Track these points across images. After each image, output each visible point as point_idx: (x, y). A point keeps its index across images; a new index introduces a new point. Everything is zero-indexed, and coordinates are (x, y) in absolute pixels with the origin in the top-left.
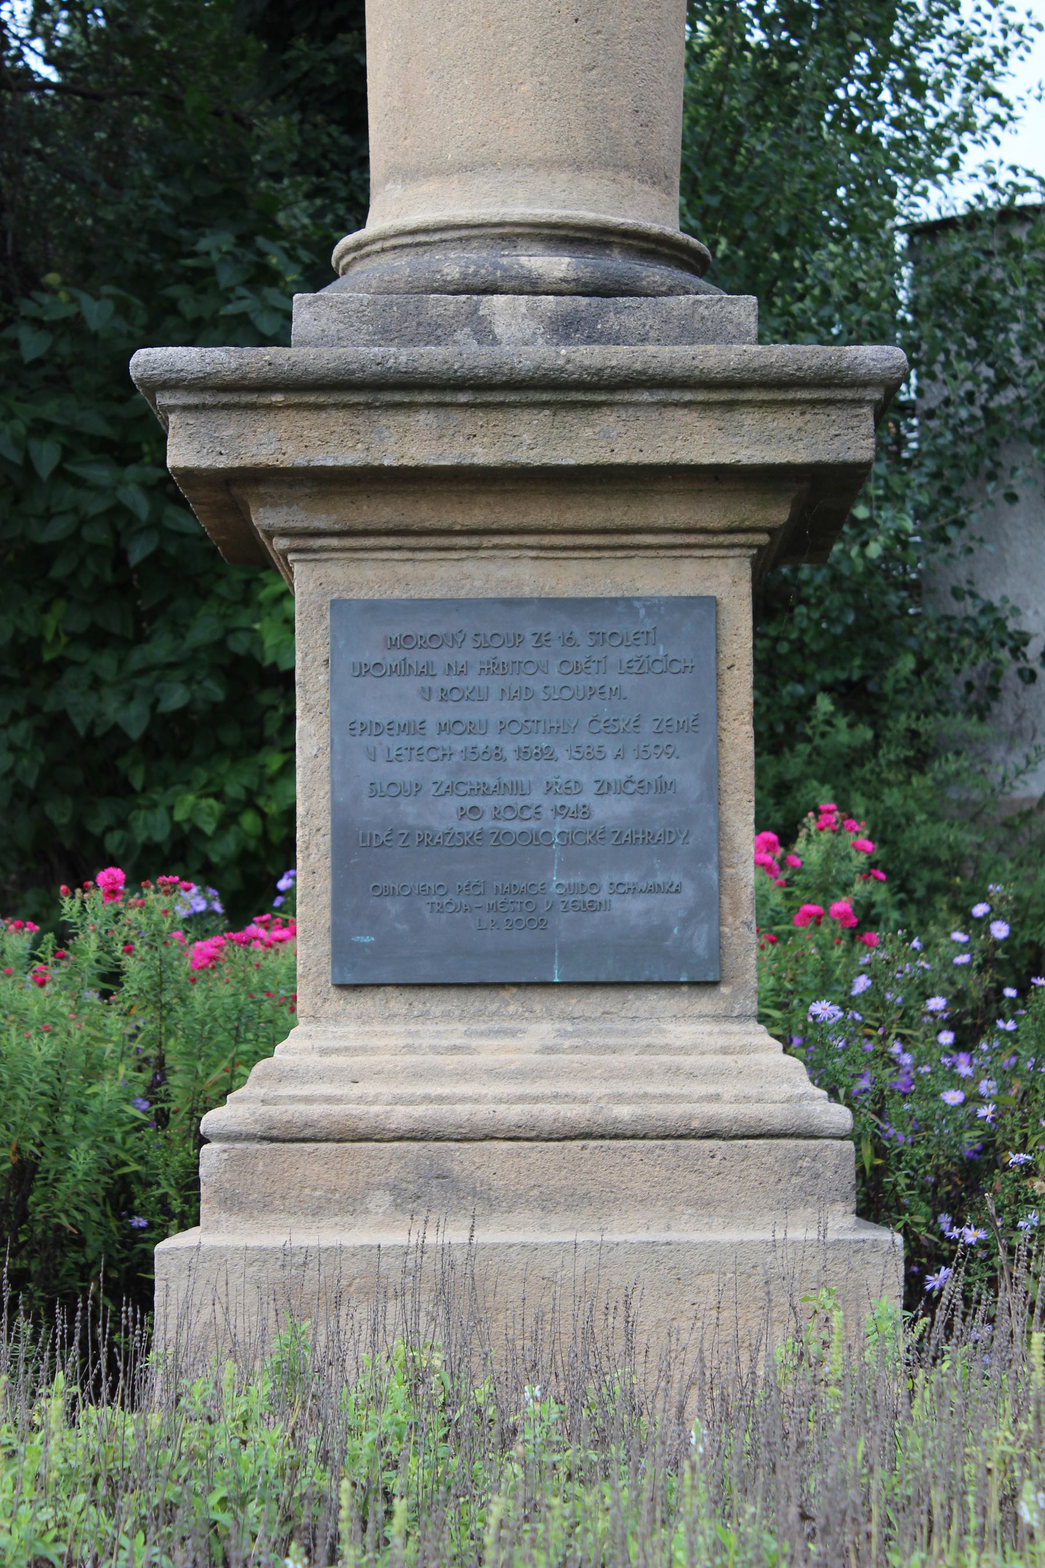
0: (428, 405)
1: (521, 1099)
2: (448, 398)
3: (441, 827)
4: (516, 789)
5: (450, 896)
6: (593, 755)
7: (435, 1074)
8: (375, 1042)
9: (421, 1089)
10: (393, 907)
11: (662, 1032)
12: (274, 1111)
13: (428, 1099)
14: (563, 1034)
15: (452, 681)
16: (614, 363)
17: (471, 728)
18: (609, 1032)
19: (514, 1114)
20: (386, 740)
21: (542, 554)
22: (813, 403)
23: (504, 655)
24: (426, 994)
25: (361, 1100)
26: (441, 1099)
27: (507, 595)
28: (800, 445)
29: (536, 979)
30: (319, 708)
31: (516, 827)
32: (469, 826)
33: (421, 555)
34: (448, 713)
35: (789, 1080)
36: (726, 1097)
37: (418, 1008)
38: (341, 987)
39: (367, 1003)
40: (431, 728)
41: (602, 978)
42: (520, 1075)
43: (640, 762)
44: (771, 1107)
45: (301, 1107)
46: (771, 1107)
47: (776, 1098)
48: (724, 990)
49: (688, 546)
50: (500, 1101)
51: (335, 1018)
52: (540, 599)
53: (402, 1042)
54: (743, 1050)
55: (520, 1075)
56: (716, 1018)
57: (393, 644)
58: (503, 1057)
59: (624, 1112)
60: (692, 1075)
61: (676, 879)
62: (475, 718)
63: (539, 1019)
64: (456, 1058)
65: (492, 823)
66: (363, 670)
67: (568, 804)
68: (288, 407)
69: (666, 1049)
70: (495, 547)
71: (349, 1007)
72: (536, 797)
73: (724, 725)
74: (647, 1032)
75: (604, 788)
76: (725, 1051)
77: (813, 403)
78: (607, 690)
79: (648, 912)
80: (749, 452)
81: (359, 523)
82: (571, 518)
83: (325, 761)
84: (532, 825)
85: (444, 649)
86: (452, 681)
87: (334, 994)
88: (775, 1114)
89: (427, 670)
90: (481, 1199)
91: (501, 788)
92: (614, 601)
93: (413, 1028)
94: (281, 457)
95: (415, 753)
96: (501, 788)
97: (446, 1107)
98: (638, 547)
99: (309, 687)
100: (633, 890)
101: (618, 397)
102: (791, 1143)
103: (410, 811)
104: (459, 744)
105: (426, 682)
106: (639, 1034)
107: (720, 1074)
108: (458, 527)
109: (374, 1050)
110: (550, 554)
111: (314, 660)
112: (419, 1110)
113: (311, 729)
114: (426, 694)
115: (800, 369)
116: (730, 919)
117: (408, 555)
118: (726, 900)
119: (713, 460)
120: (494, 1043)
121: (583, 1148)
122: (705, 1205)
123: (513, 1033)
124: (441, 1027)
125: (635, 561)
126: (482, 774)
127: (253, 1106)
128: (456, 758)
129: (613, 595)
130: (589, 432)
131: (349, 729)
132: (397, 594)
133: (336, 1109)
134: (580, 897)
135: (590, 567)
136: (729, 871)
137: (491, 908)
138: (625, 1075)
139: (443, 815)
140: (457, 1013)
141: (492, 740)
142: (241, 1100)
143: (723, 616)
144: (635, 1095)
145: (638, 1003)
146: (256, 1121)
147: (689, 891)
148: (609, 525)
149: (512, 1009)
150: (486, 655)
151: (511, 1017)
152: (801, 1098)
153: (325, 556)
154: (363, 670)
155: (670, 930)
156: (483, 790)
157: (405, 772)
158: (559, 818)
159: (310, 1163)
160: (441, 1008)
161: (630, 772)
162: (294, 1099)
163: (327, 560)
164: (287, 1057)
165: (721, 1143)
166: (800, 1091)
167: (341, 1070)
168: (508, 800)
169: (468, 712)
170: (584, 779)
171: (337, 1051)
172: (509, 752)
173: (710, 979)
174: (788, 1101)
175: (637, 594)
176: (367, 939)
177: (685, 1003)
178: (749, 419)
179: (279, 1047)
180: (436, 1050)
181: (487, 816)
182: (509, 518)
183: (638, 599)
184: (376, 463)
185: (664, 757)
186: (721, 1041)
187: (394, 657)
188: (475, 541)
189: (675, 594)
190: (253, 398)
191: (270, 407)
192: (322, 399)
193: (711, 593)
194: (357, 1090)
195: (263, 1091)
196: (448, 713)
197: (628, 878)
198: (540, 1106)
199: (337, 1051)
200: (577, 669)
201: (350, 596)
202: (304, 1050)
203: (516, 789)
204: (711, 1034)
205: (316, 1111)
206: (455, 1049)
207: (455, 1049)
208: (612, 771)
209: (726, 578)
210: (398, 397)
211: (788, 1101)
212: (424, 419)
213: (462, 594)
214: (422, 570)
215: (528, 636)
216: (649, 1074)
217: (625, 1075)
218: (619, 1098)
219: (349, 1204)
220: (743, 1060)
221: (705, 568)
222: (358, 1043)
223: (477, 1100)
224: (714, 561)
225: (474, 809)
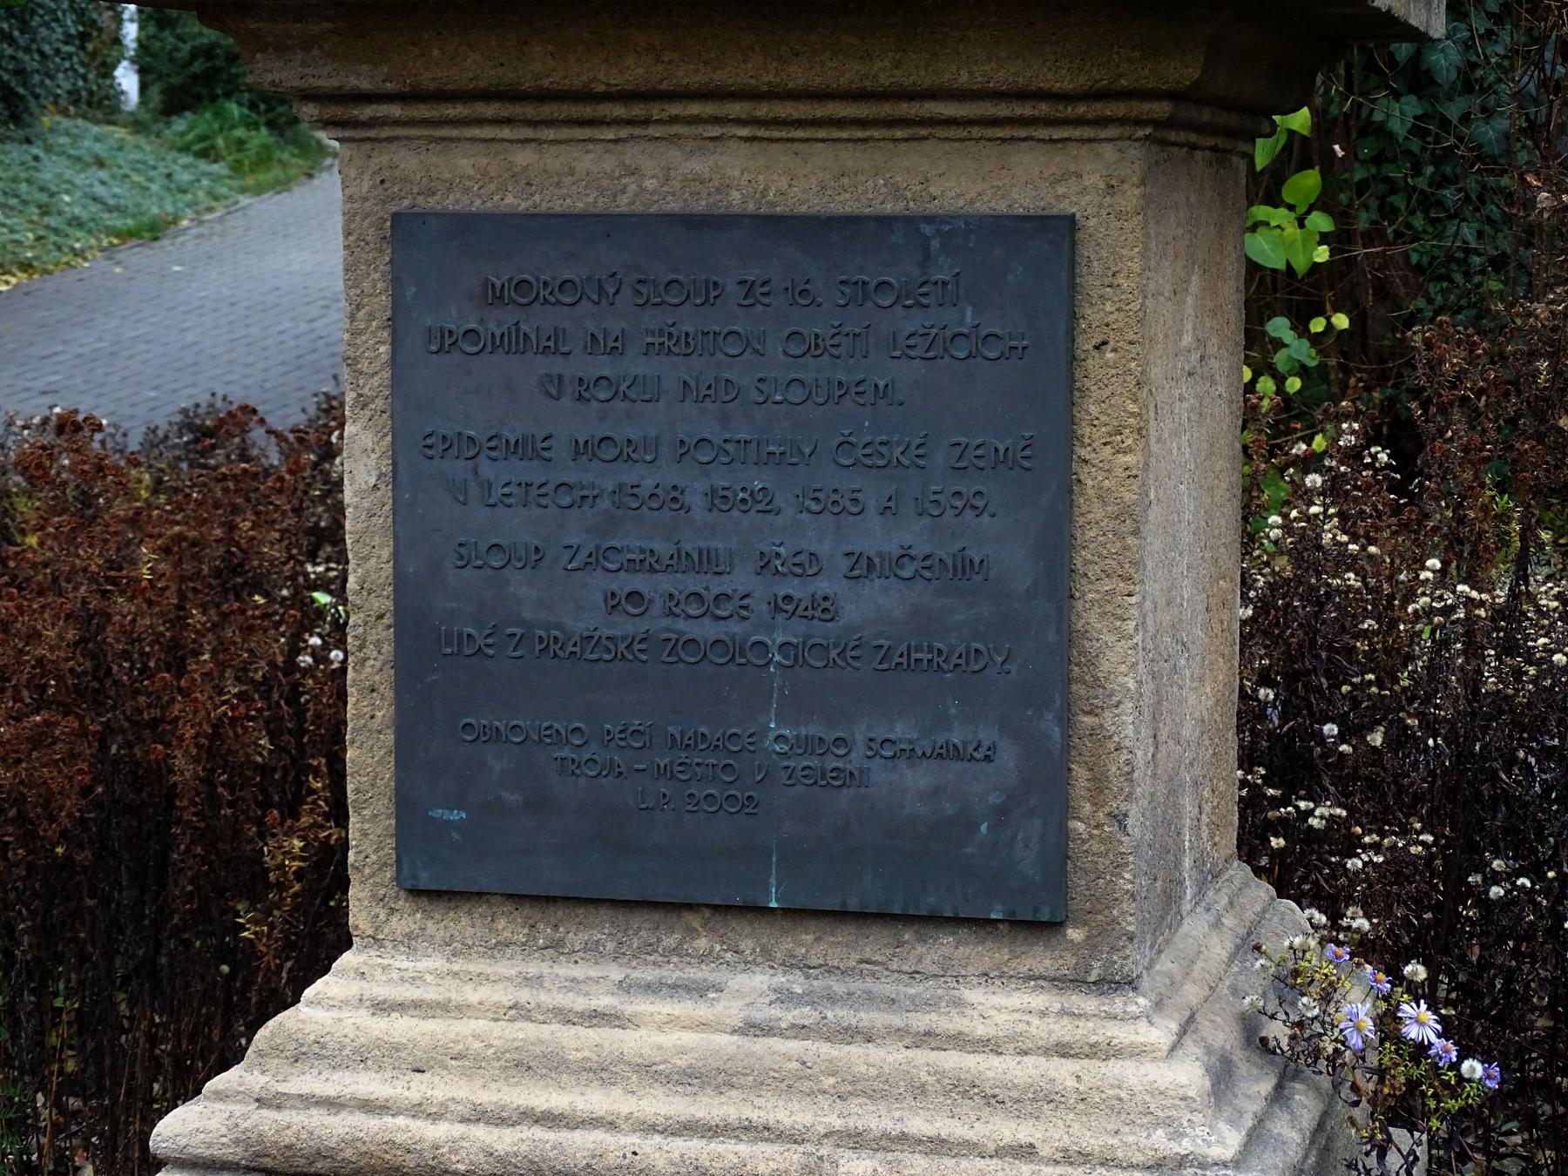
1: (688, 1128)
3: (580, 625)
4: (707, 562)
5: (593, 747)
6: (841, 508)
7: (552, 1066)
10: (497, 762)
11: (959, 1003)
12: (268, 1122)
14: (784, 997)
17: (628, 453)
18: (870, 999)
21: (761, 133)
23: (688, 321)
25: (417, 1110)
26: (550, 1119)
27: (700, 206)
29: (738, 901)
30: (380, 402)
31: (707, 630)
32: (624, 627)
33: (551, 134)
35: (1168, 1122)
36: (1045, 1151)
37: (545, 933)
38: (415, 893)
39: (463, 924)
40: (561, 451)
41: (853, 905)
42: (693, 1078)
43: (926, 520)
48: (1074, 934)
49: (1022, 122)
50: (649, 1128)
51: (409, 942)
52: (756, 217)
53: (507, 1000)
55: (693, 1078)
56: (1060, 983)
57: (494, 297)
60: (993, 1101)
61: (987, 735)
62: (634, 433)
63: (749, 965)
65: (665, 622)
66: (445, 341)
67: (797, 595)
69: (959, 1041)
70: (674, 120)
72: (741, 580)
74: (930, 1004)
75: (863, 567)
76: (1063, 1051)
78: (867, 387)
79: (937, 791)
81: (427, 79)
82: (798, 75)
84: (736, 628)
85: (586, 306)
89: (553, 345)
91: (682, 561)
92: (886, 221)
93: (533, 969)
95: (534, 491)
96: (682, 561)
99: (363, 365)
100: (910, 755)
103: (525, 592)
104: (603, 477)
105: (557, 365)
106: (918, 1005)
107: (1043, 1099)
109: (460, 1010)
111: (371, 317)
113: (367, 439)
114: (553, 386)
117: (528, 132)
118: (1080, 773)
123: (699, 991)
124: (578, 972)
125: (927, 146)
127: (238, 1109)
128: (605, 504)
129: (889, 208)
132: (512, 201)
134: (813, 762)
135: (850, 157)
137: (665, 773)
138: (878, 1090)
139: (583, 611)
140: (610, 946)
141: (669, 474)
142: (221, 1096)
143: (1086, 251)
144: (886, 1135)
145: (920, 949)
146: (237, 1142)
147: (1008, 756)
149: (702, 943)
150: (653, 319)
151: (703, 958)
153: (386, 132)
154: (445, 341)
155: (973, 827)
156: (647, 564)
157: (517, 527)
158: (780, 618)
161: (908, 539)
162: (308, 1101)
163: (390, 140)
164: (319, 1015)
168: (693, 583)
170: (824, 549)
171: (400, 1007)
172: (695, 500)
173: (1044, 916)
175: (932, 208)
176: (455, 816)
179: (309, 993)
180: (566, 1017)
181: (656, 609)
182: (689, 75)
183: (929, 219)
185: (969, 515)
187: (498, 321)
188: (638, 110)
189: (1002, 207)
193: (1065, 207)
197: (902, 730)
199: (400, 1007)
200: (816, 347)
201: (432, 203)
202: (344, 1003)
203: (707, 562)
204: (1043, 1014)
206: (596, 1018)
207: (596, 1018)
208: (876, 537)
209: (1094, 179)
213: (623, 204)
214: (554, 159)
215: (731, 287)
217: (878, 1090)
220: (1094, 1071)
221: (1058, 162)
223: (611, 1125)
224: (1073, 149)
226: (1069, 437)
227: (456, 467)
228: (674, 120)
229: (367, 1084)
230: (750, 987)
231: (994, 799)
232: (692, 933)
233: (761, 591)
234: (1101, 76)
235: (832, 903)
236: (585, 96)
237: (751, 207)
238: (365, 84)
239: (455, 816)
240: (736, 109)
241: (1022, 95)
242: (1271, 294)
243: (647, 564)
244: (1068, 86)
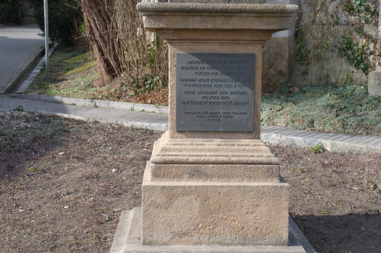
0: (198, 16)
2: (203, 14)
8: (184, 143)
9: (194, 153)
13: (195, 156)
15: (202, 71)
16: (238, 8)
19: (213, 159)
20: (188, 82)
22: (278, 16)
24: (195, 133)
25: (182, 155)
26: (198, 156)
28: (275, 25)
34: (200, 77)
41: (230, 131)
44: (264, 158)
45: (170, 157)
46: (264, 158)
47: (264, 156)
48: (254, 133)
49: (250, 43)
53: (190, 143)
54: (258, 145)
58: (210, 146)
59: (235, 159)
63: (217, 138)
64: (201, 146)
66: (183, 68)
68: (169, 15)
69: (243, 145)
71: (179, 135)
73: (256, 80)
75: (232, 93)
76: (254, 146)
77: (278, 16)
80: (265, 26)
82: (226, 38)
83: (175, 86)
86: (202, 71)
87: (176, 133)
88: (265, 159)
90: (207, 176)
91: (211, 93)
94: (168, 26)
96: (211, 93)
97: (199, 157)
98: (240, 43)
100: (237, 114)
101: (238, 15)
102: (267, 166)
105: (196, 71)
108: (203, 39)
109: (185, 145)
110: (222, 44)
111: (173, 65)
112: (195, 158)
115: (276, 10)
116: (256, 119)
117: (192, 44)
119: (257, 28)
120: (208, 143)
121: (227, 166)
122: (250, 178)
123: (212, 141)
124: (198, 140)
126: (208, 90)
130: (232, 22)
131: (181, 81)
133: (178, 157)
134: (226, 115)
136: (255, 109)
148: (234, 39)
149: (212, 136)
151: (212, 138)
152: (269, 156)
153: (175, 44)
154: (183, 68)
156: (207, 93)
157: (191, 89)
159: (173, 168)
160: (198, 136)
165: (254, 165)
166: (269, 155)
167: (178, 149)
169: (204, 77)
171: (177, 145)
172: (213, 86)
174: (267, 157)
176: (183, 122)
177: (246, 136)
178: (265, 20)
180: (197, 145)
182: (213, 38)
183: (239, 54)
184: (188, 28)
186: (253, 144)
187: (190, 65)
190: (162, 13)
191: (166, 15)
192: (177, 14)
193: (254, 53)
194: (181, 153)
195: (163, 153)
196: (200, 77)
198: (218, 158)
199: (177, 145)
203: (215, 93)
205: (174, 158)
206: (201, 145)
207: (201, 145)
208: (234, 90)
210: (192, 14)
211: (267, 157)
212: (198, 18)
213: (203, 52)
216: (239, 151)
218: (233, 156)
219: (179, 177)
220: (258, 148)
222: (181, 143)
225: (205, 97)
226: (255, 78)
227: (184, 83)
228: (210, 43)
229: (174, 153)
230: (217, 141)
231: (246, 118)
232: (210, 135)
233: (220, 96)
234: (260, 39)
235: (227, 131)
236: (201, 40)
237: (218, 53)
238: (175, 39)
239: (183, 122)
240: (218, 42)
241: (250, 40)
242: (78, 35)
243: (207, 93)
244: (256, 39)
